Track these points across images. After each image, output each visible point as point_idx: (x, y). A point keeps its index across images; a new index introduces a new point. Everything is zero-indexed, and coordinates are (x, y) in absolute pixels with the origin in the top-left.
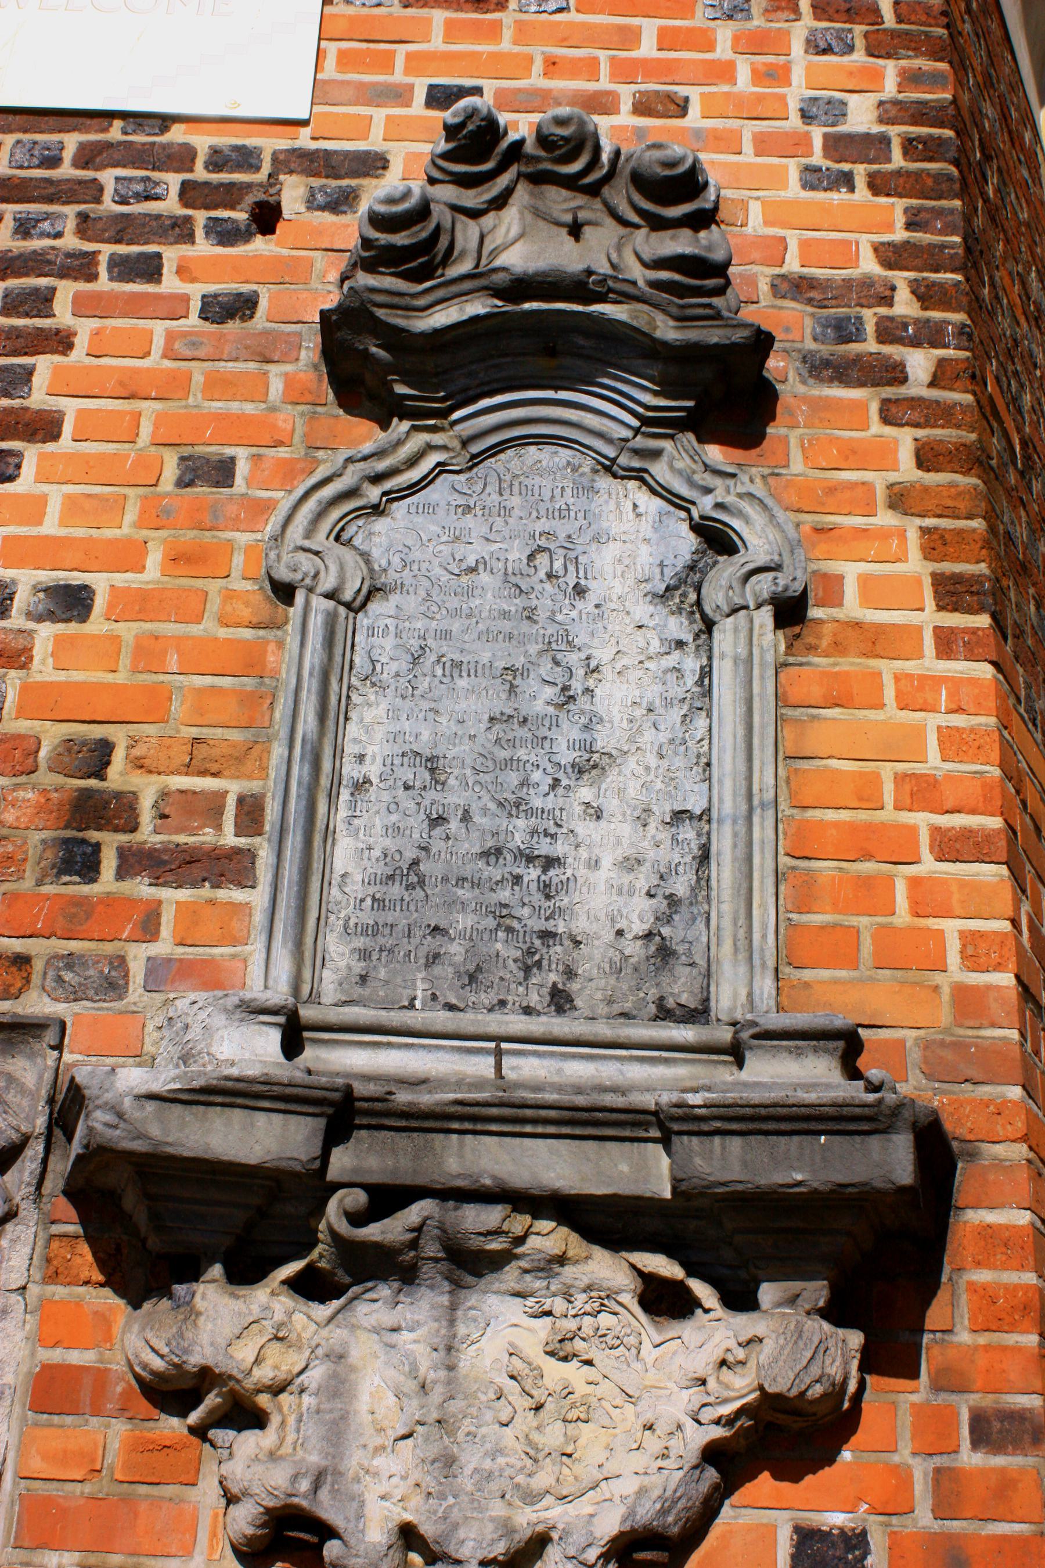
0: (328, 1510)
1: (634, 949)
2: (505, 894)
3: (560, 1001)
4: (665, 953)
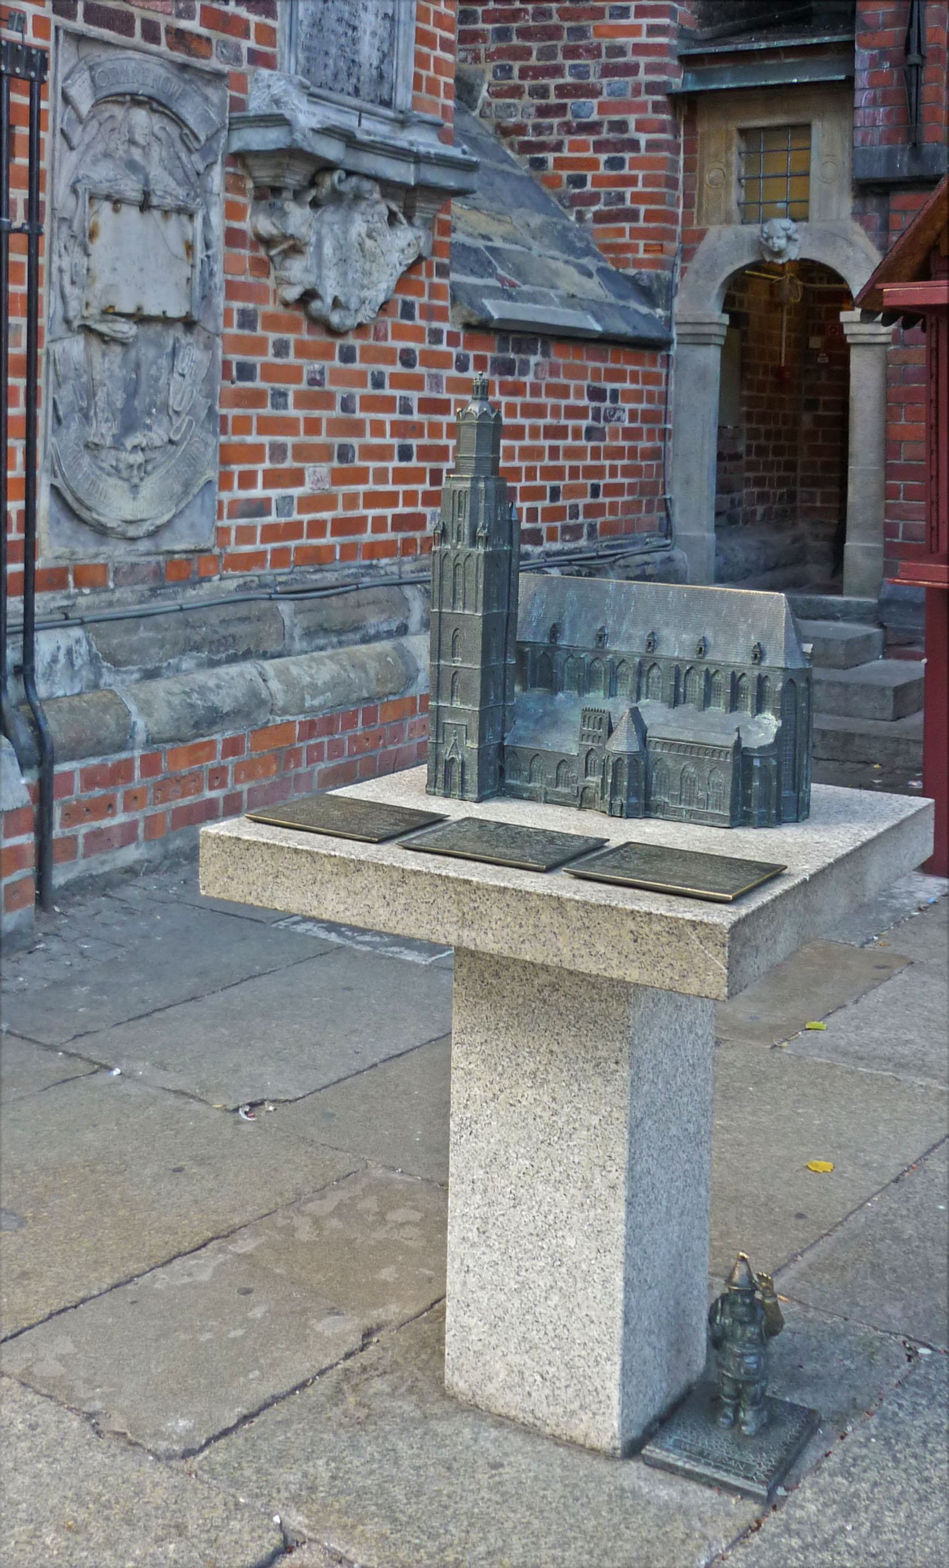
0: (320, 292)
1: (374, 72)
2: (343, 40)
3: (357, 91)
4: (381, 76)
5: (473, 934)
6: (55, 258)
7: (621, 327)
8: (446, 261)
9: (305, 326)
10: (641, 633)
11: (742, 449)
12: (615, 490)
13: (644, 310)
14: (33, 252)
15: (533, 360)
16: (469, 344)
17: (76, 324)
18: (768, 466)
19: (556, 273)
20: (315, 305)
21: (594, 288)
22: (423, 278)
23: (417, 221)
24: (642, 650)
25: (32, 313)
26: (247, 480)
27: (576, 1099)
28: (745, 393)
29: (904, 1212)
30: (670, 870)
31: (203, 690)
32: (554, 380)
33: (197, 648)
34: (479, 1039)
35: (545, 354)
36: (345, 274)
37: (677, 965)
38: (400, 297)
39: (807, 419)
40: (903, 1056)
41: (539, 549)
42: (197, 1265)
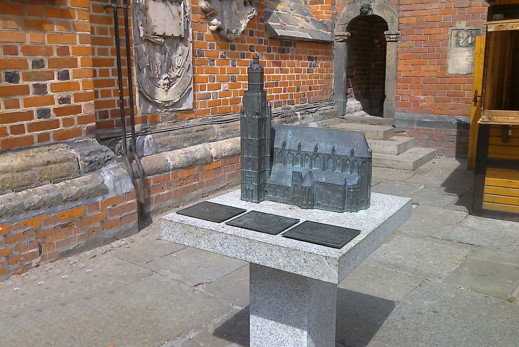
0: (223, 28)
5: (250, 257)
6: (135, 17)
7: (318, 38)
8: (263, 17)
9: (219, 39)
10: (313, 145)
11: (354, 74)
12: (316, 88)
13: (325, 32)
14: (126, 15)
15: (291, 48)
16: (271, 44)
17: (143, 39)
18: (362, 79)
19: (298, 21)
20: (221, 32)
21: (310, 26)
22: (256, 23)
23: (253, 4)
24: (313, 151)
25: (128, 35)
26: (203, 88)
27: (290, 303)
28: (355, 57)
29: (398, 319)
30: (319, 233)
31: (191, 152)
32: (298, 55)
33: (189, 139)
34: (258, 282)
35: (295, 46)
36: (231, 22)
37: (320, 271)
38: (249, 29)
39: (373, 65)
40: (398, 264)
41: (293, 106)
42: (176, 343)
